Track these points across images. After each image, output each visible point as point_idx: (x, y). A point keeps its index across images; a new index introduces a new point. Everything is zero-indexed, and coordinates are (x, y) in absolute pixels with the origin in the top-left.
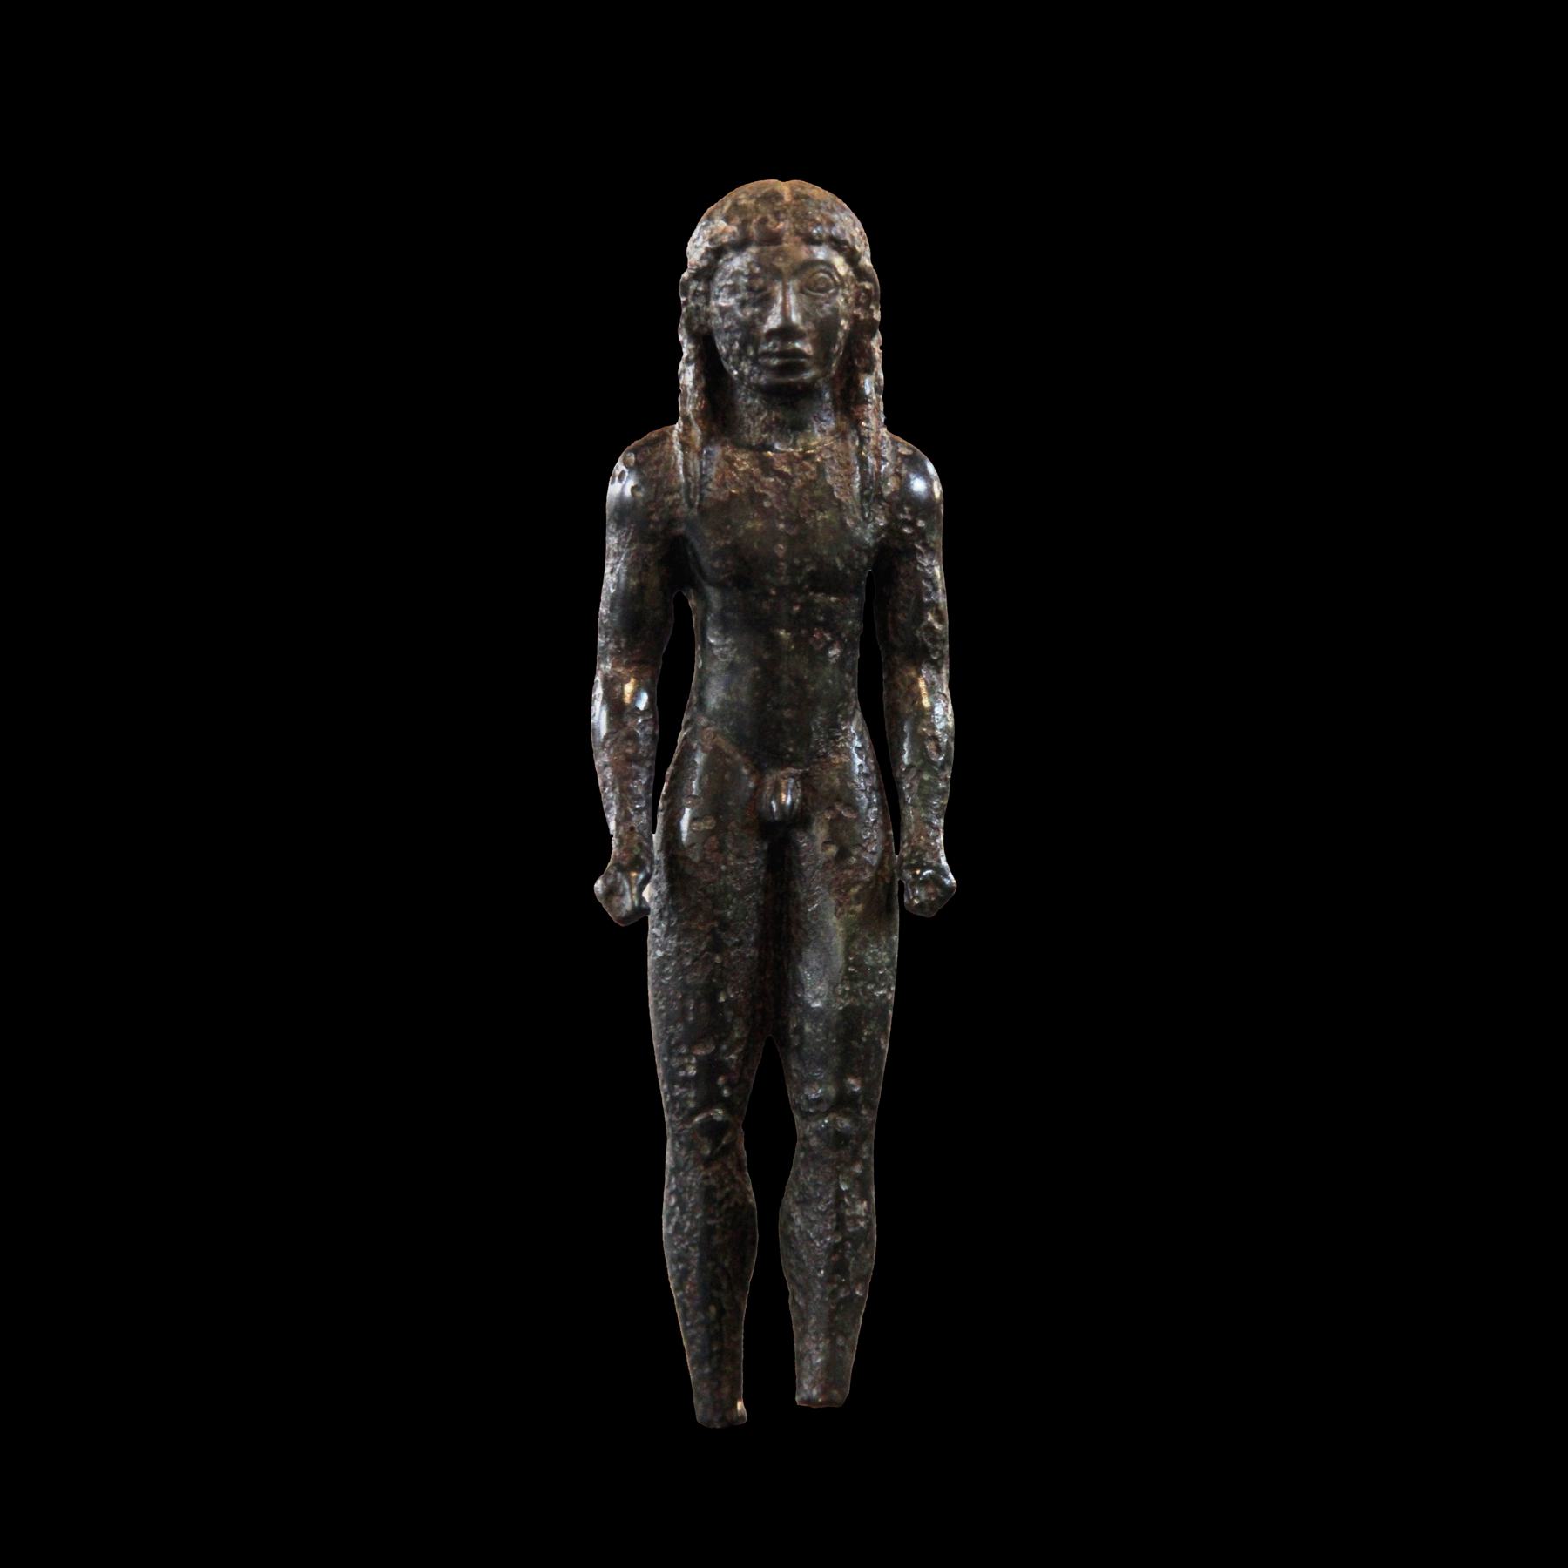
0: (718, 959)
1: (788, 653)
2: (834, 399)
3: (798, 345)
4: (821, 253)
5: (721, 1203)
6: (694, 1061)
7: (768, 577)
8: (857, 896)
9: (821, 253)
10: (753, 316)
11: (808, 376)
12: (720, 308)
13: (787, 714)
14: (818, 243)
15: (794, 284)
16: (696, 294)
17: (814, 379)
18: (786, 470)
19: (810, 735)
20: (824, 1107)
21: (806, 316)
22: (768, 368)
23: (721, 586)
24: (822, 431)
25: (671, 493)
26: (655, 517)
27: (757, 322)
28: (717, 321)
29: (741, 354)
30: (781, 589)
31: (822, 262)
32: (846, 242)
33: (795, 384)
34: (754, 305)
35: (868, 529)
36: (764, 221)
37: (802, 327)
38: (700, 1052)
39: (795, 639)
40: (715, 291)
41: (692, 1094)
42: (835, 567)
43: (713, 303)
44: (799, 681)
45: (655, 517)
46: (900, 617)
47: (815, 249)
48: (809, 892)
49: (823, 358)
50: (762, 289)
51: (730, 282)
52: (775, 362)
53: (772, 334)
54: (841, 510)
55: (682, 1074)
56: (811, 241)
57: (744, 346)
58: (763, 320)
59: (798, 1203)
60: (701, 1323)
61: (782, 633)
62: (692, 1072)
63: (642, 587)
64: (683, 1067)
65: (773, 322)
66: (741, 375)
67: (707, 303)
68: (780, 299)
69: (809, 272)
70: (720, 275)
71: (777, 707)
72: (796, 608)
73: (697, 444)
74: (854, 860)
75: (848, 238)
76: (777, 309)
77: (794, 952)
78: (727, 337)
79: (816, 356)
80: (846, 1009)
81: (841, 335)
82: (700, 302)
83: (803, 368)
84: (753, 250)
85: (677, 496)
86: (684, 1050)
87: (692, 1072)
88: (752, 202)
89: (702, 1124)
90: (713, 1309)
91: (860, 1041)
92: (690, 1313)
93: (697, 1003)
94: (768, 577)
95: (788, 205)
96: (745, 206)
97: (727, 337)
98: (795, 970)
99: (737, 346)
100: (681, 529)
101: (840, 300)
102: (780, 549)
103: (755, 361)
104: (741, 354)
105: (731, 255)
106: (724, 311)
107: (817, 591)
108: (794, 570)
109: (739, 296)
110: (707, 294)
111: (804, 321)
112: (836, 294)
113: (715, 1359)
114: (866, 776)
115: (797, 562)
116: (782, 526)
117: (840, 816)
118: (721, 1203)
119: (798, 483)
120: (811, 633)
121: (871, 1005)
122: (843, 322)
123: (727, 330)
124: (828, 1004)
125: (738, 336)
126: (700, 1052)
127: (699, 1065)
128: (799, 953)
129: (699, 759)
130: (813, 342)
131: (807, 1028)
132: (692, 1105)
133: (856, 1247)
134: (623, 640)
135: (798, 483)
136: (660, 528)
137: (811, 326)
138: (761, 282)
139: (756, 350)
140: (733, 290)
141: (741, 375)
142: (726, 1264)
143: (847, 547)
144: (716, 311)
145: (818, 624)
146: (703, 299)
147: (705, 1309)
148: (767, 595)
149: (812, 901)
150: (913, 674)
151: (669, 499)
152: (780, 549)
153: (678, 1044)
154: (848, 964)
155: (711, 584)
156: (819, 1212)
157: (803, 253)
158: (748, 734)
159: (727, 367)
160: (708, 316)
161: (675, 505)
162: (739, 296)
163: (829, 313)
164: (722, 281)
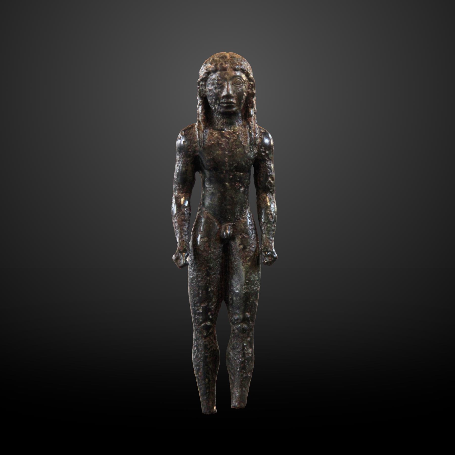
0: (208, 278)
1: (229, 190)
2: (242, 116)
3: (231, 100)
4: (238, 73)
5: (209, 349)
6: (201, 308)
7: (223, 167)
8: (249, 260)
9: (238, 73)
10: (218, 92)
11: (234, 109)
12: (209, 89)
13: (228, 207)
14: (237, 70)
15: (230, 82)
16: (202, 85)
17: (236, 110)
18: (228, 136)
19: (235, 213)
20: (239, 321)
21: (234, 92)
22: (223, 107)
23: (209, 170)
24: (239, 125)
25: (195, 143)
26: (190, 150)
27: (220, 93)
28: (208, 93)
29: (215, 103)
30: (227, 171)
31: (239, 76)
32: (245, 70)
33: (231, 111)
34: (219, 89)
35: (252, 153)
36: (222, 64)
37: (233, 95)
38: (203, 305)
39: (231, 186)
40: (208, 84)
41: (201, 318)
42: (242, 164)
43: (207, 88)
44: (232, 198)
45: (190, 150)
46: (261, 179)
47: (237, 72)
48: (235, 259)
49: (239, 104)
50: (221, 84)
51: (212, 82)
52: (225, 105)
53: (224, 97)
54: (244, 148)
55: (198, 312)
56: (235, 70)
57: (216, 100)
58: (222, 93)
59: (231, 349)
60: (203, 384)
61: (227, 184)
62: (201, 311)
63: (186, 170)
64: (198, 310)
65: (224, 93)
66: (215, 109)
67: (205, 88)
68: (226, 87)
69: (235, 79)
70: (209, 80)
71: (226, 205)
72: (231, 177)
73: (202, 129)
74: (248, 250)
75: (246, 69)
76: (225, 90)
77: (230, 276)
78: (211, 98)
79: (237, 103)
80: (245, 293)
81: (244, 97)
82: (203, 88)
83: (233, 107)
84: (219, 72)
85: (196, 144)
86: (198, 305)
87: (201, 311)
88: (218, 59)
89: (204, 326)
90: (207, 380)
91: (250, 302)
92: (200, 381)
93: (202, 291)
94: (223, 167)
95: (229, 59)
96: (216, 60)
97: (211, 98)
98: (231, 282)
99: (214, 100)
100: (198, 154)
101: (244, 87)
102: (226, 159)
103: (219, 105)
104: (215, 103)
105: (212, 74)
106: (210, 90)
107: (237, 171)
108: (230, 165)
109: (214, 86)
110: (205, 85)
111: (233, 93)
112: (242, 85)
113: (207, 394)
114: (251, 225)
115: (231, 163)
116: (227, 153)
117: (244, 237)
118: (209, 349)
119: (232, 140)
120: (235, 184)
121: (253, 292)
122: (245, 93)
123: (211, 96)
124: (240, 291)
125: (214, 97)
126: (203, 305)
127: (203, 309)
128: (232, 277)
129: (203, 220)
130: (236, 99)
131: (234, 298)
132: (201, 321)
133: (248, 362)
134: (181, 186)
135: (232, 140)
136: (192, 153)
137: (235, 95)
138: (221, 82)
139: (219, 102)
140: (213, 84)
141: (215, 109)
142: (211, 367)
143: (246, 159)
144: (208, 90)
145: (237, 181)
146: (204, 87)
147: (205, 380)
148: (222, 173)
149: (236, 262)
150: (265, 195)
151: (194, 145)
152: (226, 159)
153: (197, 303)
154: (246, 280)
155: (206, 169)
156: (238, 352)
157: (233, 73)
158: (217, 213)
159: (211, 106)
160: (206, 92)
161: (196, 146)
162: (214, 86)
163: (241, 91)
164: (209, 81)
